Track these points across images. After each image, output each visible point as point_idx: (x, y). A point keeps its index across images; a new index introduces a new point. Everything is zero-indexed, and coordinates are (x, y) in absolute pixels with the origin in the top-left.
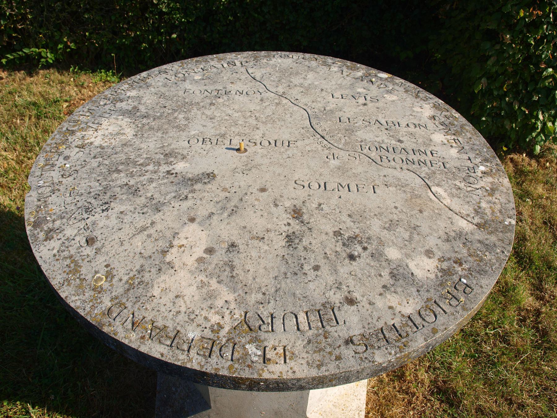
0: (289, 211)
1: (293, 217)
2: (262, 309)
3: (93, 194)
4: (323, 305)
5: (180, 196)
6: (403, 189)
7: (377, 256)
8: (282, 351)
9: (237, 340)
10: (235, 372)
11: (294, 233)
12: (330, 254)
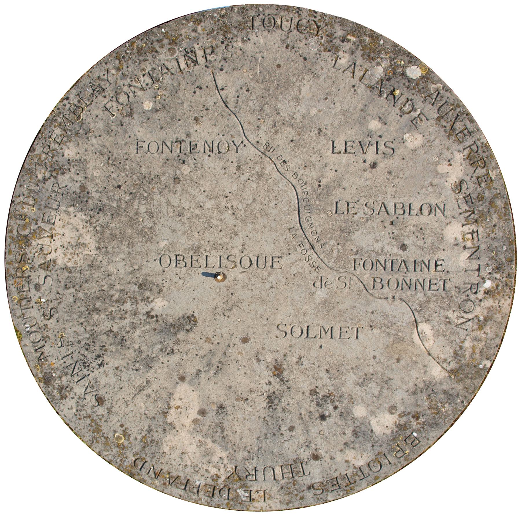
1: (274, 375)
3: (83, 343)
4: (295, 461)
5: (166, 349)
6: (388, 330)
7: (346, 415)
8: (263, 493)
9: (231, 486)
11: (274, 393)
12: (304, 415)
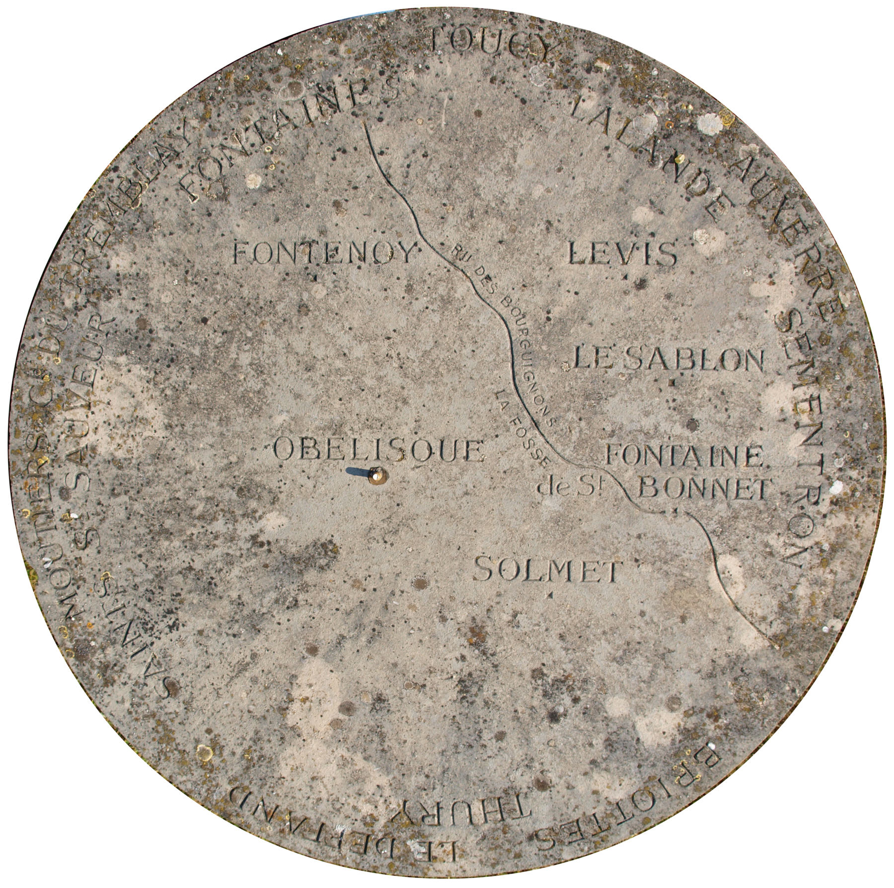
0: (463, 630)
1: (471, 644)
2: (426, 797)
3: (142, 589)
4: (506, 792)
5: (285, 599)
6: (665, 567)
7: (592, 712)
8: (451, 847)
9: (396, 835)
10: (396, 870)
11: (470, 674)
12: (522, 713)
